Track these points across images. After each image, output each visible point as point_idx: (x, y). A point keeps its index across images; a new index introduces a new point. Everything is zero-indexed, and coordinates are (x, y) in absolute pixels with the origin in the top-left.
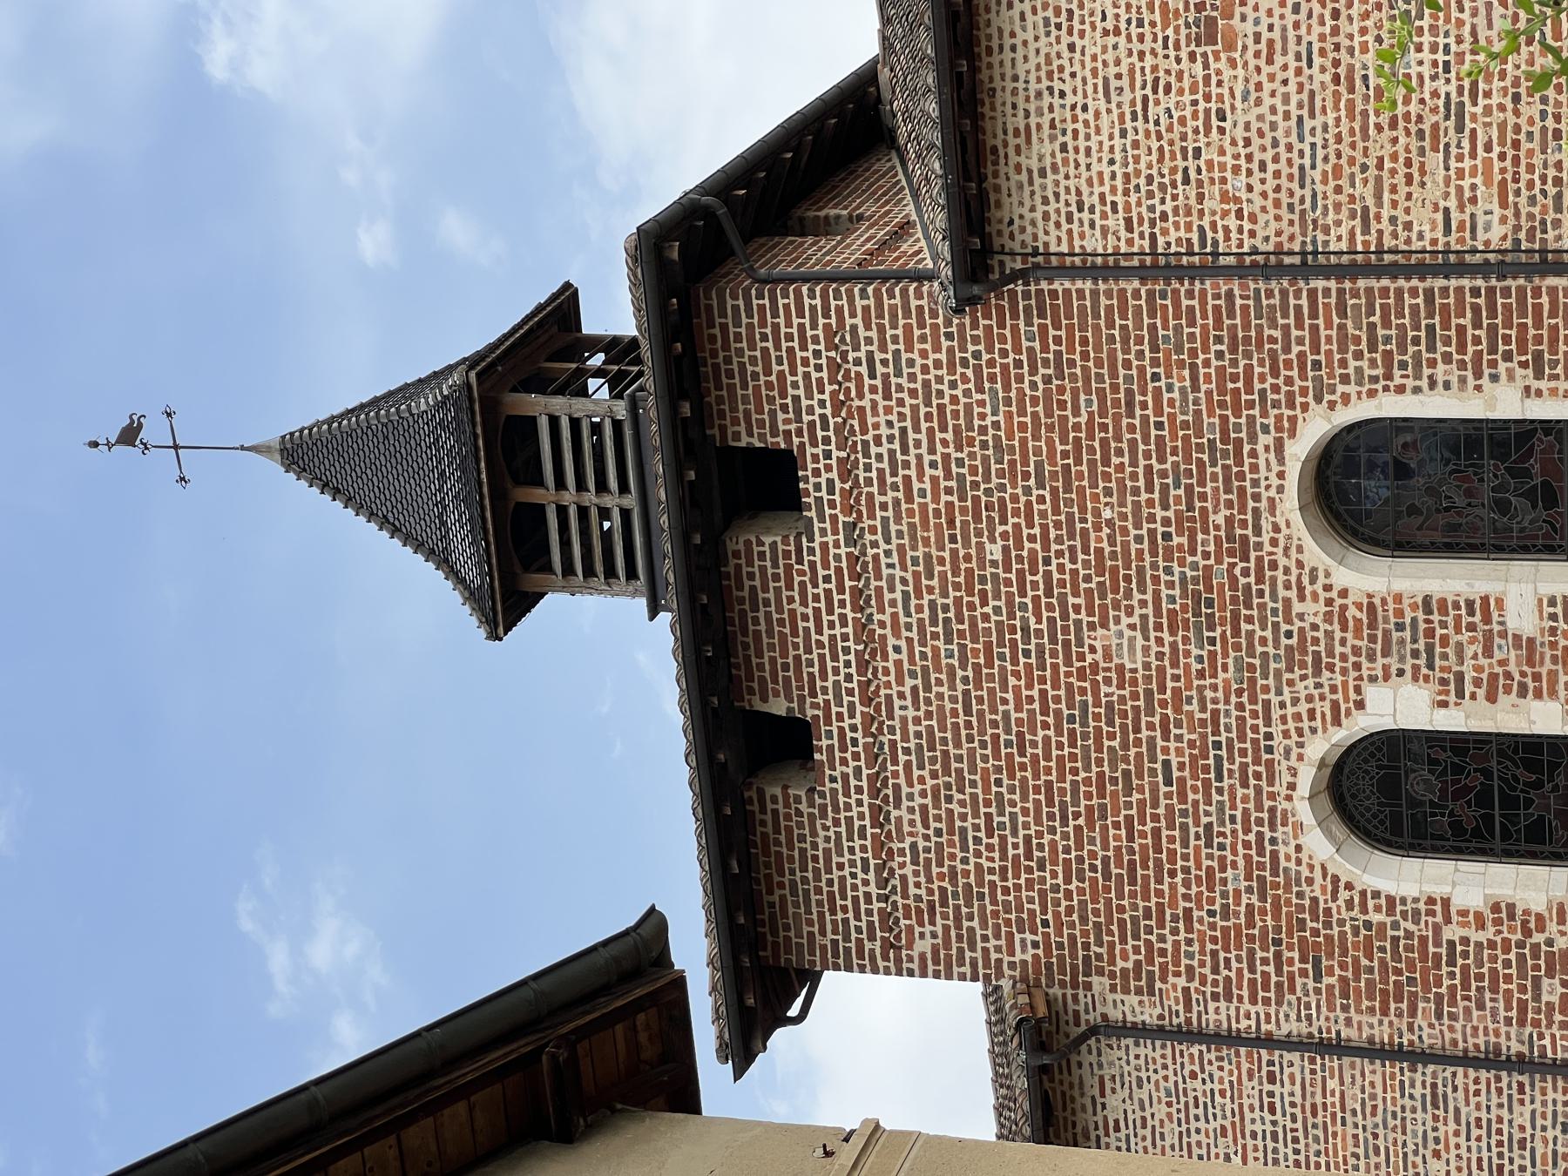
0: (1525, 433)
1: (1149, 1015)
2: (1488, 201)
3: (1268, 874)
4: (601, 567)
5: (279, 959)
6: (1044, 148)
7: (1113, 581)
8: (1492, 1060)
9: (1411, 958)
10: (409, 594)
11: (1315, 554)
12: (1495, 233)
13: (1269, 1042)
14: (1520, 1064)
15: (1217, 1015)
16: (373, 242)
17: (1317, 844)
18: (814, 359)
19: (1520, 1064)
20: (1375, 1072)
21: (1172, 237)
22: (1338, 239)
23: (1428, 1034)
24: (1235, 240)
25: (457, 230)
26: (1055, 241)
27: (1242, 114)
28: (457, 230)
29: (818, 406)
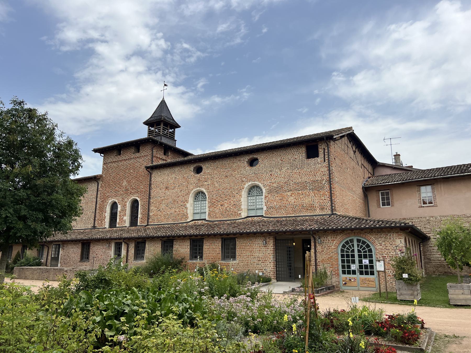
0: (137, 217)
1: (99, 187)
2: (153, 213)
3: (108, 197)
4: (150, 132)
5: (244, 90)
6: (159, 174)
7: (129, 182)
8: (95, 217)
9: (102, 210)
10: (148, 113)
11: (130, 200)
12: (151, 214)
13: (97, 198)
14: (95, 219)
15: (99, 193)
16: (316, 92)
17: (110, 201)
18: (146, 154)
19: (95, 219)
20: (95, 207)
21: (152, 186)
22: (151, 200)
23: (97, 211)
24: (152, 191)
25: (318, 100)
26: (153, 175)
27: (160, 191)
28: (318, 100)
29: (143, 154)
